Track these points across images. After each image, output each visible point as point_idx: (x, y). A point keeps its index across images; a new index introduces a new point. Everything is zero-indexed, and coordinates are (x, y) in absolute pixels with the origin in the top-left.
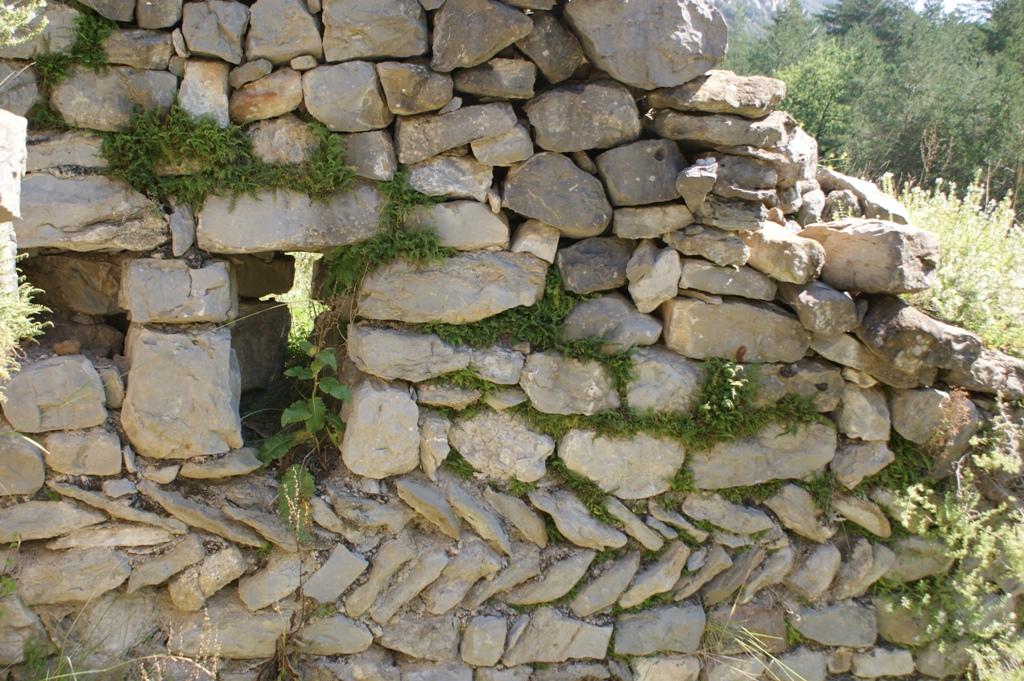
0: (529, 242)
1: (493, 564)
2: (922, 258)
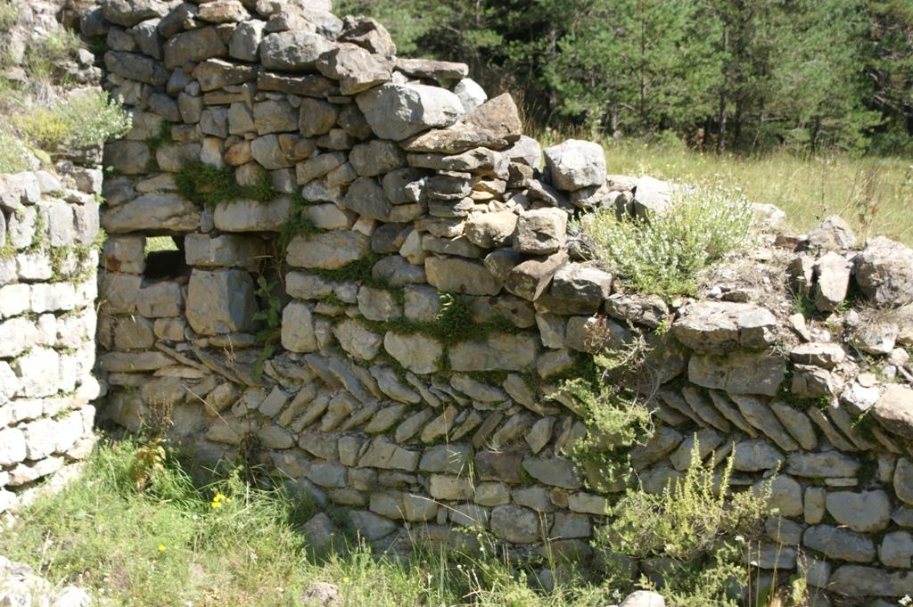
0: (358, 226)
1: (350, 406)
2: (535, 231)
